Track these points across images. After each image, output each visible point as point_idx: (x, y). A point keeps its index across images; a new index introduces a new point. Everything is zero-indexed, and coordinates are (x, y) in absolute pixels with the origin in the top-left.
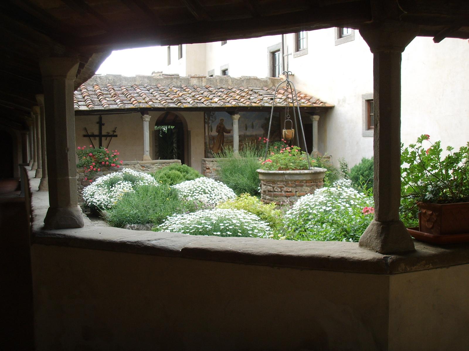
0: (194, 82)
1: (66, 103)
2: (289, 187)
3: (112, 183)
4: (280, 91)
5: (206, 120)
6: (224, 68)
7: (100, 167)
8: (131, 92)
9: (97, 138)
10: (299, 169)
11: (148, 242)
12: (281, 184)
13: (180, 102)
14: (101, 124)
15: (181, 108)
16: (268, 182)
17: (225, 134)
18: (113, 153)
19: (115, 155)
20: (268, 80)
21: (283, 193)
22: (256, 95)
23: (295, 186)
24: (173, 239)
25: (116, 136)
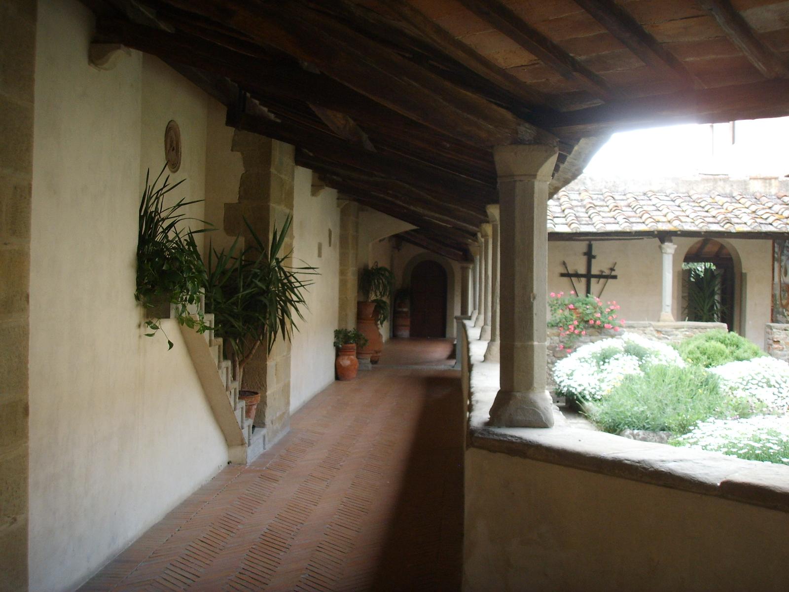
0: (756, 187)
3: (604, 358)
5: (776, 255)
7: (585, 328)
9: (583, 280)
11: (661, 464)
14: (589, 256)
15: (730, 233)
19: (612, 310)
24: (711, 463)
25: (615, 277)
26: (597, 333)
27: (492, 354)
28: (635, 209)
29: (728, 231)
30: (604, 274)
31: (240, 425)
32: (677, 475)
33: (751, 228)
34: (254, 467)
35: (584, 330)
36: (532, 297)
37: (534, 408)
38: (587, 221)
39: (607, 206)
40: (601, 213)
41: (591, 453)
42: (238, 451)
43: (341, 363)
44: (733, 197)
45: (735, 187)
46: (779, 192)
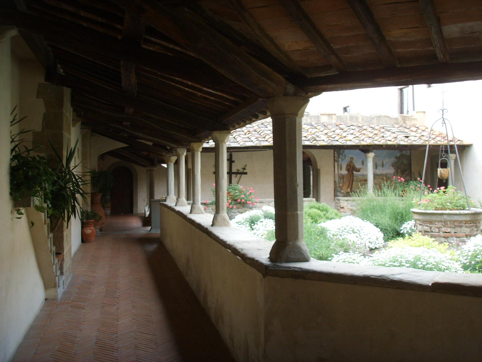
0: (324, 119)
1: (297, 140)
2: (448, 227)
3: (252, 222)
4: (412, 129)
5: (336, 159)
6: (345, 106)
7: (235, 204)
8: (263, 129)
10: (456, 209)
12: (439, 224)
13: (314, 140)
15: (316, 146)
16: (425, 223)
17: (355, 172)
18: (248, 190)
19: (250, 193)
20: (399, 117)
21: (441, 233)
22: (389, 133)
23: (454, 226)
25: (246, 173)
26: (242, 207)
27: (218, 221)
28: (259, 133)
29: (315, 145)
30: (239, 172)
31: (55, 274)
32: (405, 281)
33: (328, 143)
34: (63, 301)
35: (234, 205)
36: (296, 186)
37: (300, 250)
38: (233, 140)
39: (243, 131)
40: (241, 135)
41: (349, 274)
42: (52, 292)
43: (85, 232)
44: (312, 125)
45: (313, 119)
46: (337, 122)
